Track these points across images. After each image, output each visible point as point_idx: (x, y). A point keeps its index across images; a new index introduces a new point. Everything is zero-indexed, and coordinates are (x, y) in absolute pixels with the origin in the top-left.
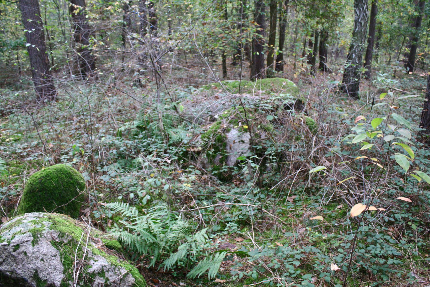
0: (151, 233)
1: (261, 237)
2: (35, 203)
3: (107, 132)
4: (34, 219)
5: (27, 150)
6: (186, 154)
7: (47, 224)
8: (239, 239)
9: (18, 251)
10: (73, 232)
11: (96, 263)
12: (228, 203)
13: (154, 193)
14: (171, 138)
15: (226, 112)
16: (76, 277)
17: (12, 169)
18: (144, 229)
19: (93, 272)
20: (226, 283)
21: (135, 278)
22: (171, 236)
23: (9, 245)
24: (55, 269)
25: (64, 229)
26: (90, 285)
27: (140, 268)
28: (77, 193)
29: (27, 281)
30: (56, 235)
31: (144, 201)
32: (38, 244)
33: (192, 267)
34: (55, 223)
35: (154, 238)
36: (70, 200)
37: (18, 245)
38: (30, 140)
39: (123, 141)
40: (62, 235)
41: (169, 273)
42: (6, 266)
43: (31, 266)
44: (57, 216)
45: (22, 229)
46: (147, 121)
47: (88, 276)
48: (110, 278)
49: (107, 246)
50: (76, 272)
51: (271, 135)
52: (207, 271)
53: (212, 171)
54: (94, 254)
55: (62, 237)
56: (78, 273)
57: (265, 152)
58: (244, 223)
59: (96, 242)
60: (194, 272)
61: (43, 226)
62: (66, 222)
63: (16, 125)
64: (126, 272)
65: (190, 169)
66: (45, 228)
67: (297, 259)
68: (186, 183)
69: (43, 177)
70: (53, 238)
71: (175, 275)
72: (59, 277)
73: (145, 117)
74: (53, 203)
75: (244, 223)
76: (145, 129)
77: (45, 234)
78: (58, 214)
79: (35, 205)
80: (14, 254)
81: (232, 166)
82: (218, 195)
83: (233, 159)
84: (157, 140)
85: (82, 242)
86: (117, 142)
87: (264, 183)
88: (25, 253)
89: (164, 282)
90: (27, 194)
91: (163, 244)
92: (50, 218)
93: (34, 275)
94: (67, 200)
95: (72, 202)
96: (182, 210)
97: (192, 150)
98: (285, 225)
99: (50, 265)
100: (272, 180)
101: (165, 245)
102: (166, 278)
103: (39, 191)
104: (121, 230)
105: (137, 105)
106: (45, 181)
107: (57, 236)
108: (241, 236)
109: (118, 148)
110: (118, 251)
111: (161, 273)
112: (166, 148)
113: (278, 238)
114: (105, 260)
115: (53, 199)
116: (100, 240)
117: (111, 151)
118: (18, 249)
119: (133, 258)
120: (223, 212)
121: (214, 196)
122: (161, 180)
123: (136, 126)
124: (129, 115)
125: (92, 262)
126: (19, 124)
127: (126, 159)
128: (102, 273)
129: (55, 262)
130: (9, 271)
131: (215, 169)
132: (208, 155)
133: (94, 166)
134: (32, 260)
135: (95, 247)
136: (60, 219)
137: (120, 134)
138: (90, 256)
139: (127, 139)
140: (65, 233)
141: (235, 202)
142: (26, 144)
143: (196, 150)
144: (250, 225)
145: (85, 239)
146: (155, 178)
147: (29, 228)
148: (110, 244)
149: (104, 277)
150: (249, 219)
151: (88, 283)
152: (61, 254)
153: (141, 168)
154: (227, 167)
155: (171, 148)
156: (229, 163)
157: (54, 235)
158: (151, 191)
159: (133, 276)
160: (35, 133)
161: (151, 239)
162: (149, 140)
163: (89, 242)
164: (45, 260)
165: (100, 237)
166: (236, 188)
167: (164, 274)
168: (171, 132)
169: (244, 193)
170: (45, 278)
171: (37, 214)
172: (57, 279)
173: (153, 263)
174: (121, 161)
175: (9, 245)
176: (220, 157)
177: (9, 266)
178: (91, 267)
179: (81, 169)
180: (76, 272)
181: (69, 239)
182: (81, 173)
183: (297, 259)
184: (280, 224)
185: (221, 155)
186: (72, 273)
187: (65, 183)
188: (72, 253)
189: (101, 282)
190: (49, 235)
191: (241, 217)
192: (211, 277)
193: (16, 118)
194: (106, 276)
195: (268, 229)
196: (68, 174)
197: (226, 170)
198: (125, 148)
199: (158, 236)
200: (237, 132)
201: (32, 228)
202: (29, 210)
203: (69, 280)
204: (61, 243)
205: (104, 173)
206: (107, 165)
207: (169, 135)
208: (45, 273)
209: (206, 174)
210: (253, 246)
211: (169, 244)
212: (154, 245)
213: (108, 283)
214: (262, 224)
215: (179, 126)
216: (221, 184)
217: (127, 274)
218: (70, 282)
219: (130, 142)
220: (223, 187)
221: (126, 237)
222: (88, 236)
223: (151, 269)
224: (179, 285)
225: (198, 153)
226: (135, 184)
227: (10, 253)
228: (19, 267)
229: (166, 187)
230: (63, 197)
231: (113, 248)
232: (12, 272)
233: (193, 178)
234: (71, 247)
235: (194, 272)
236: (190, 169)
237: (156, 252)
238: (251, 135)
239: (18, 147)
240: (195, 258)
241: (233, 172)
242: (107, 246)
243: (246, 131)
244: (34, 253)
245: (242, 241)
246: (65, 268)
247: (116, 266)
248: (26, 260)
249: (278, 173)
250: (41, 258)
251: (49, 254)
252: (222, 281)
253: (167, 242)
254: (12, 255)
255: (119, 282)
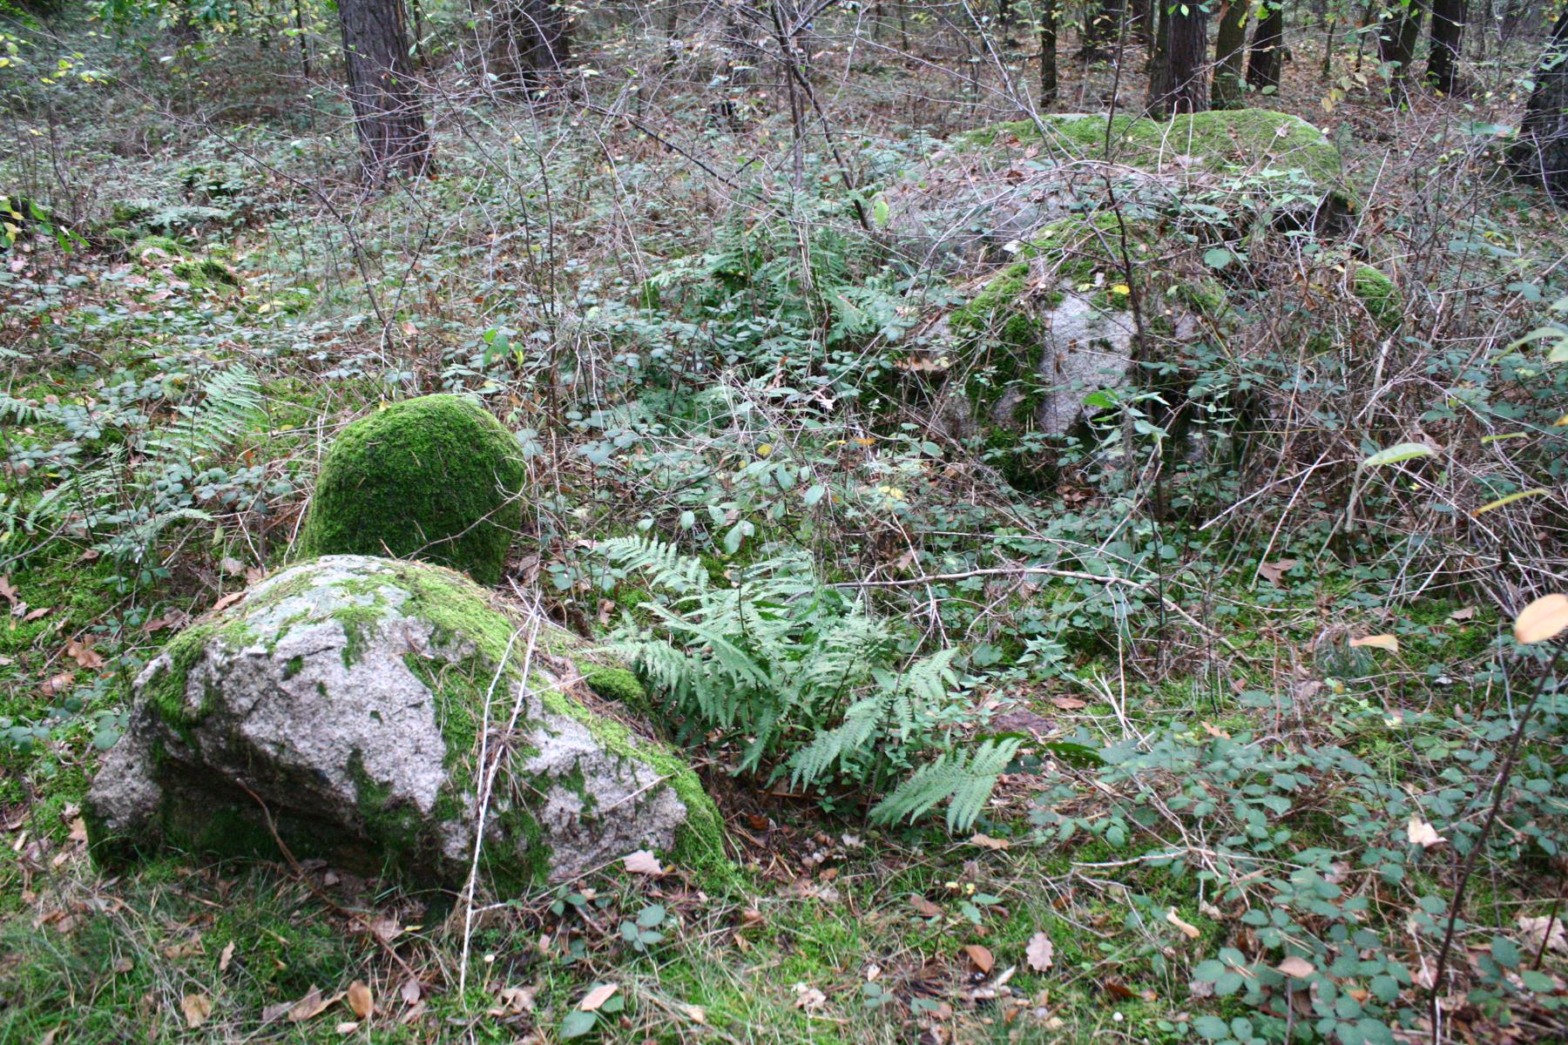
0: (749, 650)
1: (1149, 700)
2: (355, 526)
3: (606, 290)
4: (351, 576)
5: (327, 344)
6: (889, 379)
7: (394, 595)
8: (1068, 703)
9: (297, 679)
10: (480, 631)
11: (553, 742)
12: (1036, 568)
13: (769, 516)
14: (837, 320)
15: (1049, 233)
16: (485, 781)
17: (279, 406)
18: (725, 637)
19: (544, 773)
20: (1010, 851)
21: (688, 804)
22: (821, 668)
23: (269, 656)
24: (418, 751)
25: (449, 616)
26: (533, 815)
27: (704, 774)
28: (495, 500)
29: (326, 781)
30: (421, 637)
31: (732, 542)
32: (362, 660)
33: (889, 785)
34: (418, 596)
35: (761, 673)
36: (471, 521)
37: (298, 659)
38: (338, 309)
39: (665, 324)
40: (442, 636)
41: (806, 799)
42: (261, 724)
43: (339, 732)
44: (429, 575)
45: (313, 607)
46: (753, 254)
47: (526, 783)
48: (600, 798)
49: (593, 687)
50: (486, 766)
51: (1216, 325)
52: (943, 804)
53: (983, 450)
54: (548, 709)
55: (442, 644)
56: (493, 768)
57: (1187, 387)
58: (1091, 644)
59: (558, 671)
60: (893, 806)
61: (378, 600)
62: (454, 595)
63: (294, 256)
64: (657, 780)
65: (902, 437)
66: (385, 609)
67: (1282, 792)
68: (890, 485)
69: (381, 435)
70: (410, 646)
71: (828, 809)
72: (433, 775)
73: (748, 240)
74: (411, 527)
75: (1091, 644)
76: (743, 282)
77: (386, 630)
78: (429, 566)
79: (354, 531)
80: (287, 686)
81: (1061, 435)
82: (1002, 536)
83: (1063, 412)
84: (784, 325)
85: (510, 667)
86: (642, 326)
87: (1176, 503)
88: (322, 688)
89: (786, 829)
90: (326, 494)
91: (790, 695)
92: (402, 577)
93: (350, 763)
94: (460, 522)
95: (478, 530)
96: (866, 581)
97: (915, 367)
98: (1245, 665)
99: (402, 735)
100: (1206, 495)
101: (800, 699)
102: (796, 817)
103: (368, 484)
104: (645, 635)
105: (720, 195)
106: (388, 452)
107: (424, 640)
108: (1076, 689)
109: (643, 349)
110: (630, 709)
111: (777, 798)
112: (818, 355)
113: (1214, 709)
114: (586, 735)
115: (412, 513)
116: (569, 664)
117: (619, 358)
118: (297, 672)
119: (682, 734)
120: (1016, 600)
121: (985, 542)
122: (795, 469)
123: (711, 269)
124: (687, 230)
125: (540, 736)
126: (303, 252)
127: (670, 387)
128: (572, 777)
129: (416, 725)
130: (273, 743)
131: (995, 442)
132: (973, 388)
133: (557, 414)
134: (343, 713)
135: (554, 688)
136: (437, 583)
137: (654, 300)
138: (536, 715)
139: (678, 315)
140: (450, 632)
141: (1061, 567)
142: (326, 323)
143: (928, 366)
144: (1111, 654)
145: (519, 656)
146: (776, 459)
147: (334, 605)
148: (605, 680)
149: (580, 790)
150: (1109, 629)
151: (527, 808)
152: (438, 703)
153: (725, 423)
154: (1040, 436)
155: (836, 355)
156: (1051, 422)
157: (416, 635)
158: (759, 507)
159: (680, 796)
160: (355, 286)
161: (749, 675)
162: (757, 325)
163: (532, 667)
164: (383, 715)
165: (571, 654)
166: (1068, 516)
167: (785, 803)
168: (840, 297)
169: (1096, 537)
170: (385, 778)
171: (358, 560)
172: (423, 783)
173: (752, 758)
174: (654, 396)
175: (269, 656)
176: (1018, 399)
177: (271, 727)
178: (537, 754)
179: (511, 417)
180: (486, 766)
181: (467, 651)
182: (513, 430)
183: (1282, 792)
184: (1225, 658)
185: (1022, 390)
186: (474, 767)
187: (454, 462)
188: (473, 701)
189: (569, 807)
190: (397, 634)
191: (1079, 622)
192: (956, 826)
193: (294, 231)
194: (587, 789)
195: (1177, 675)
196: (465, 429)
197: (1036, 447)
198: (669, 347)
199: (774, 665)
200: (1086, 308)
201: (344, 605)
202: (335, 545)
203: (461, 791)
204: (438, 664)
205: (592, 432)
206: (602, 407)
207: (830, 308)
208: (385, 760)
209: (962, 458)
210: (1116, 731)
211: (811, 698)
212: (760, 696)
213: (594, 813)
214: (1155, 654)
215: (869, 280)
216: (1013, 499)
217: (660, 788)
218: (465, 797)
219: (690, 328)
220: (1022, 509)
221: (664, 662)
222: (531, 647)
223: (743, 781)
224: (841, 842)
225: (937, 379)
226: (701, 479)
227: (272, 682)
228: (302, 731)
229: (813, 495)
230: (447, 509)
231: (615, 697)
232: (281, 747)
233: (912, 466)
234: (471, 680)
235: (893, 806)
236: (902, 437)
237: (766, 721)
238: (1138, 322)
239: (301, 334)
240: (903, 754)
241: (1063, 455)
242: (593, 687)
243: (1120, 304)
244: (348, 689)
245: (1077, 710)
246: (450, 749)
247: (622, 758)
248: (323, 712)
249: (1232, 473)
250: (371, 708)
251: (399, 699)
252: (996, 844)
253: (805, 691)
254: (279, 690)
255: (629, 814)
